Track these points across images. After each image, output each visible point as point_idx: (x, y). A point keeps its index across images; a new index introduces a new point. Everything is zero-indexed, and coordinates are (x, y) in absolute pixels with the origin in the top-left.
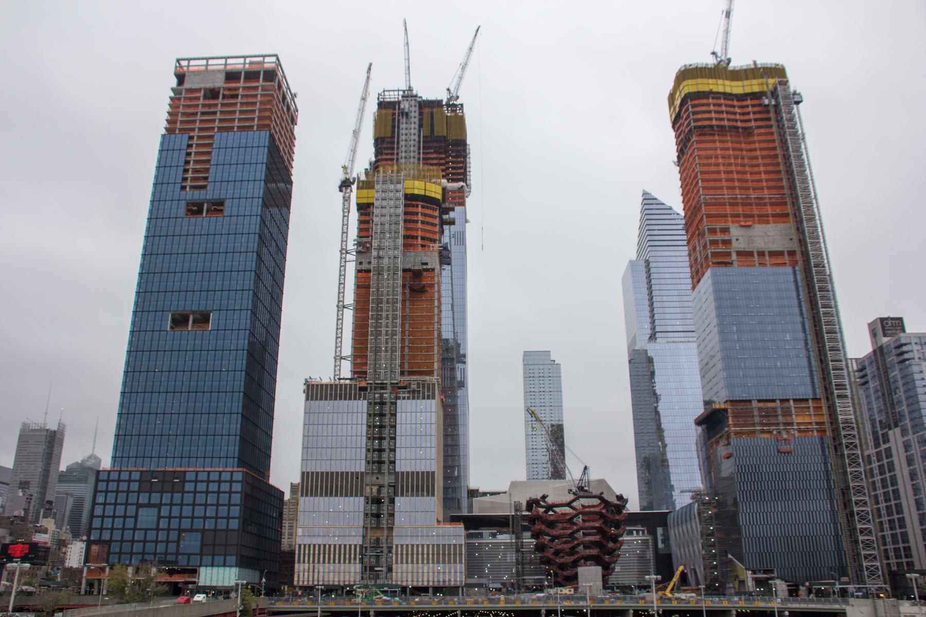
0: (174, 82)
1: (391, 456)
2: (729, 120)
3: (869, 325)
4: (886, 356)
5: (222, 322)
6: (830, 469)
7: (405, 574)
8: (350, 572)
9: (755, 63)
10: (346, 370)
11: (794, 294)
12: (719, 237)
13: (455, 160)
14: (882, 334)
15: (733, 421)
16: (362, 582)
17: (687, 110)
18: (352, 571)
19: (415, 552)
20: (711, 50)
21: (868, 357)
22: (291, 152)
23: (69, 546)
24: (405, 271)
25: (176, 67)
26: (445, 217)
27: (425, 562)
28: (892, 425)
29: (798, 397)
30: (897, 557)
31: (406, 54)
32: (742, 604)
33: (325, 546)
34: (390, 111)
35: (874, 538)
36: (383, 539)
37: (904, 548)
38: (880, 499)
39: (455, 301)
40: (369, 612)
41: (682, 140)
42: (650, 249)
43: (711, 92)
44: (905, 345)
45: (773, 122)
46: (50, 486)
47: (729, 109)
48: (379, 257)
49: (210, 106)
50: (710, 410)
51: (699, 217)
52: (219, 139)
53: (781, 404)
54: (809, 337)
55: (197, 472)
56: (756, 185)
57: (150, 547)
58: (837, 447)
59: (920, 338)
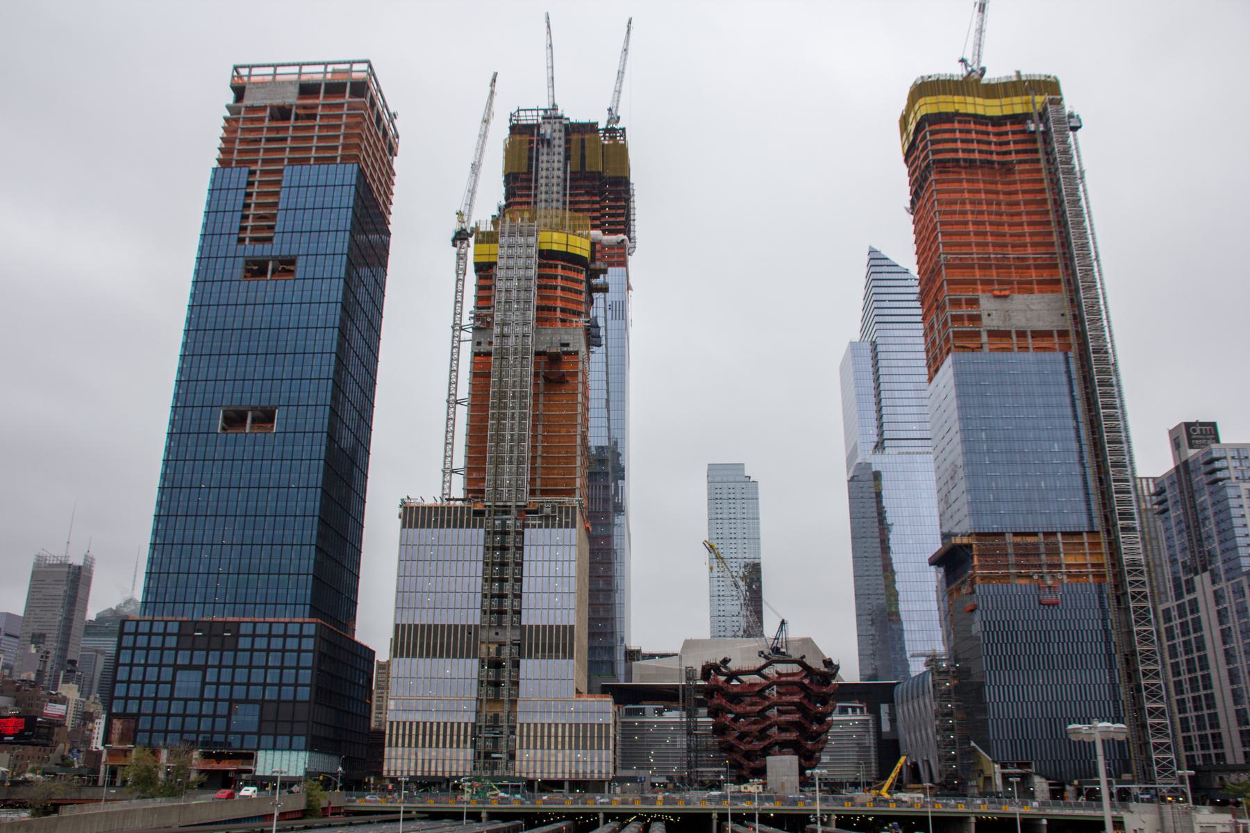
0: (230, 97)
1: (515, 603)
2: (980, 152)
3: (1171, 432)
4: (1193, 476)
5: (291, 422)
6: (1110, 628)
7: (532, 764)
8: (458, 760)
9: (1018, 73)
10: (458, 488)
11: (1066, 389)
12: (964, 311)
13: (613, 204)
15: (979, 561)
16: (474, 773)
17: (924, 137)
18: (462, 758)
19: (546, 734)
20: (960, 57)
21: (1168, 476)
22: (388, 193)
23: (97, 721)
24: (538, 354)
25: (233, 77)
26: (594, 281)
27: (560, 747)
29: (1068, 530)
30: (1203, 748)
31: (549, 60)
32: (984, 809)
33: (425, 724)
34: (526, 138)
35: (1168, 722)
36: (503, 716)
37: (1213, 735)
38: (1182, 668)
39: (612, 395)
40: (480, 813)
41: (916, 180)
42: (877, 326)
43: (957, 114)
44: (1218, 459)
45: (1041, 155)
46: (73, 640)
47: (980, 137)
48: (503, 336)
49: (278, 130)
50: (948, 546)
52: (290, 174)
53: (1045, 539)
54: (1085, 448)
55: (255, 623)
56: (1017, 241)
57: (191, 723)
58: (1120, 598)
59: (1238, 450)
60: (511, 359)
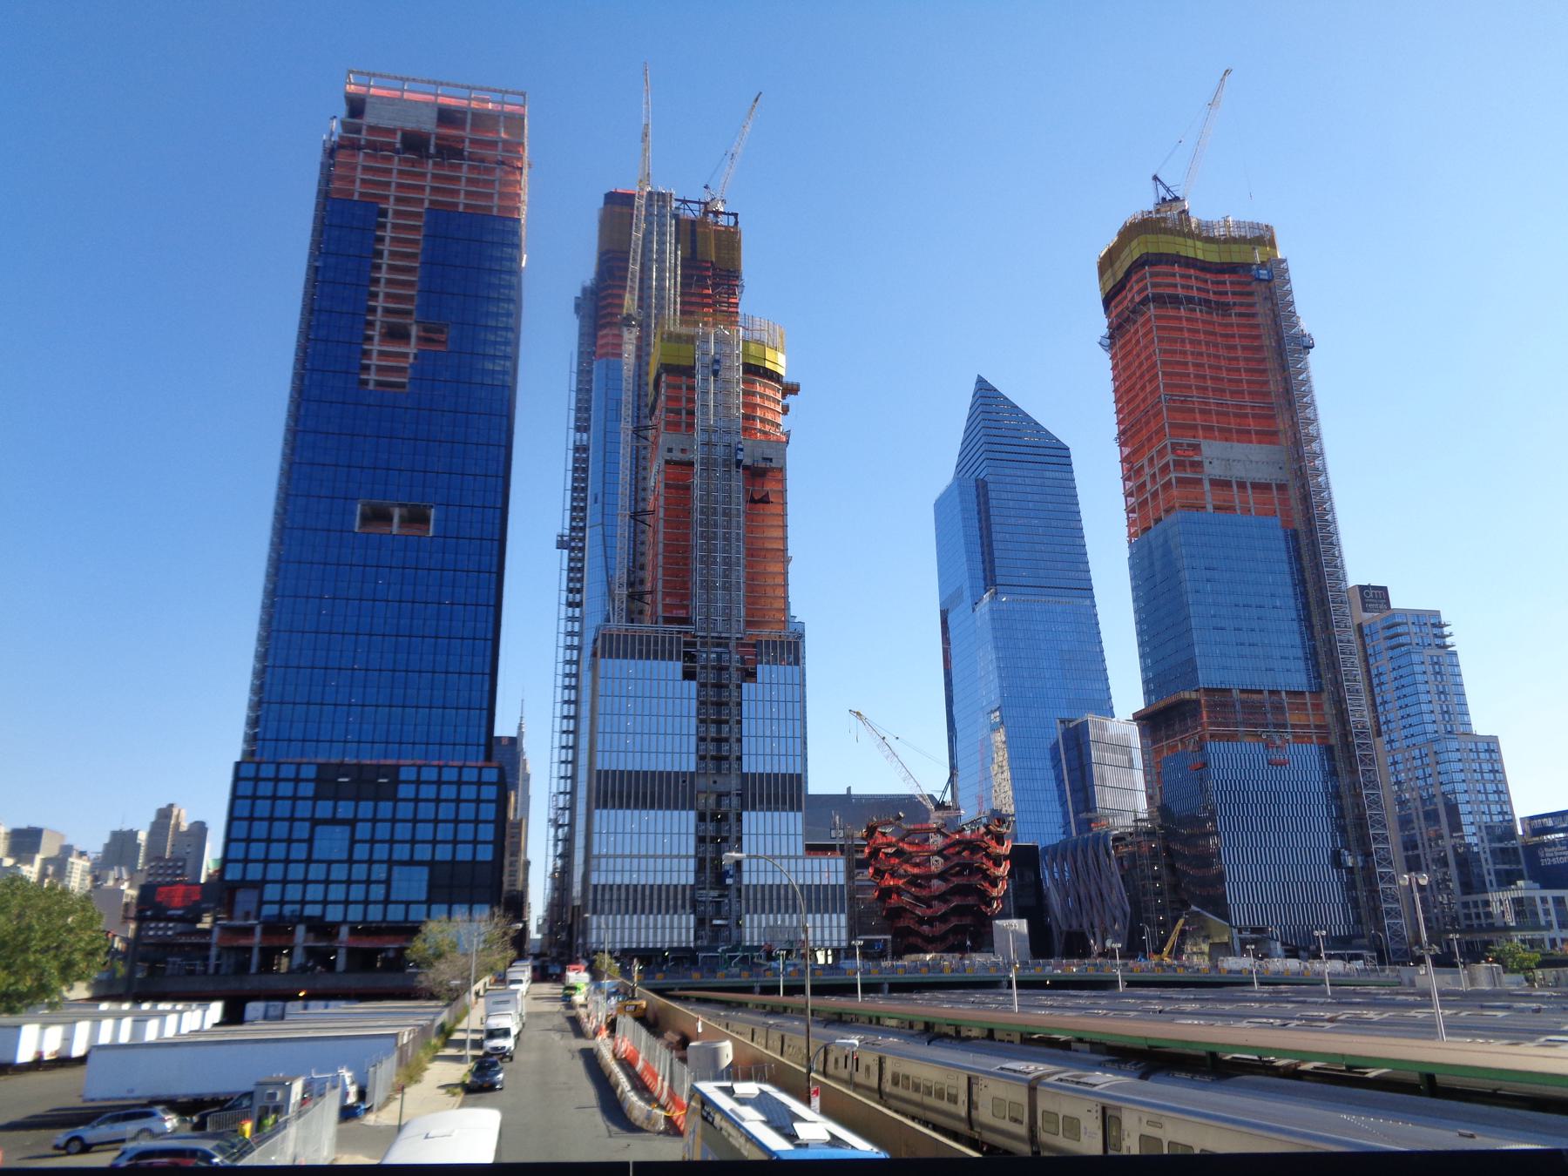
0: (342, 110)
15: (1209, 718)
29: (1245, 687)
44: (1399, 624)
59: (1418, 616)
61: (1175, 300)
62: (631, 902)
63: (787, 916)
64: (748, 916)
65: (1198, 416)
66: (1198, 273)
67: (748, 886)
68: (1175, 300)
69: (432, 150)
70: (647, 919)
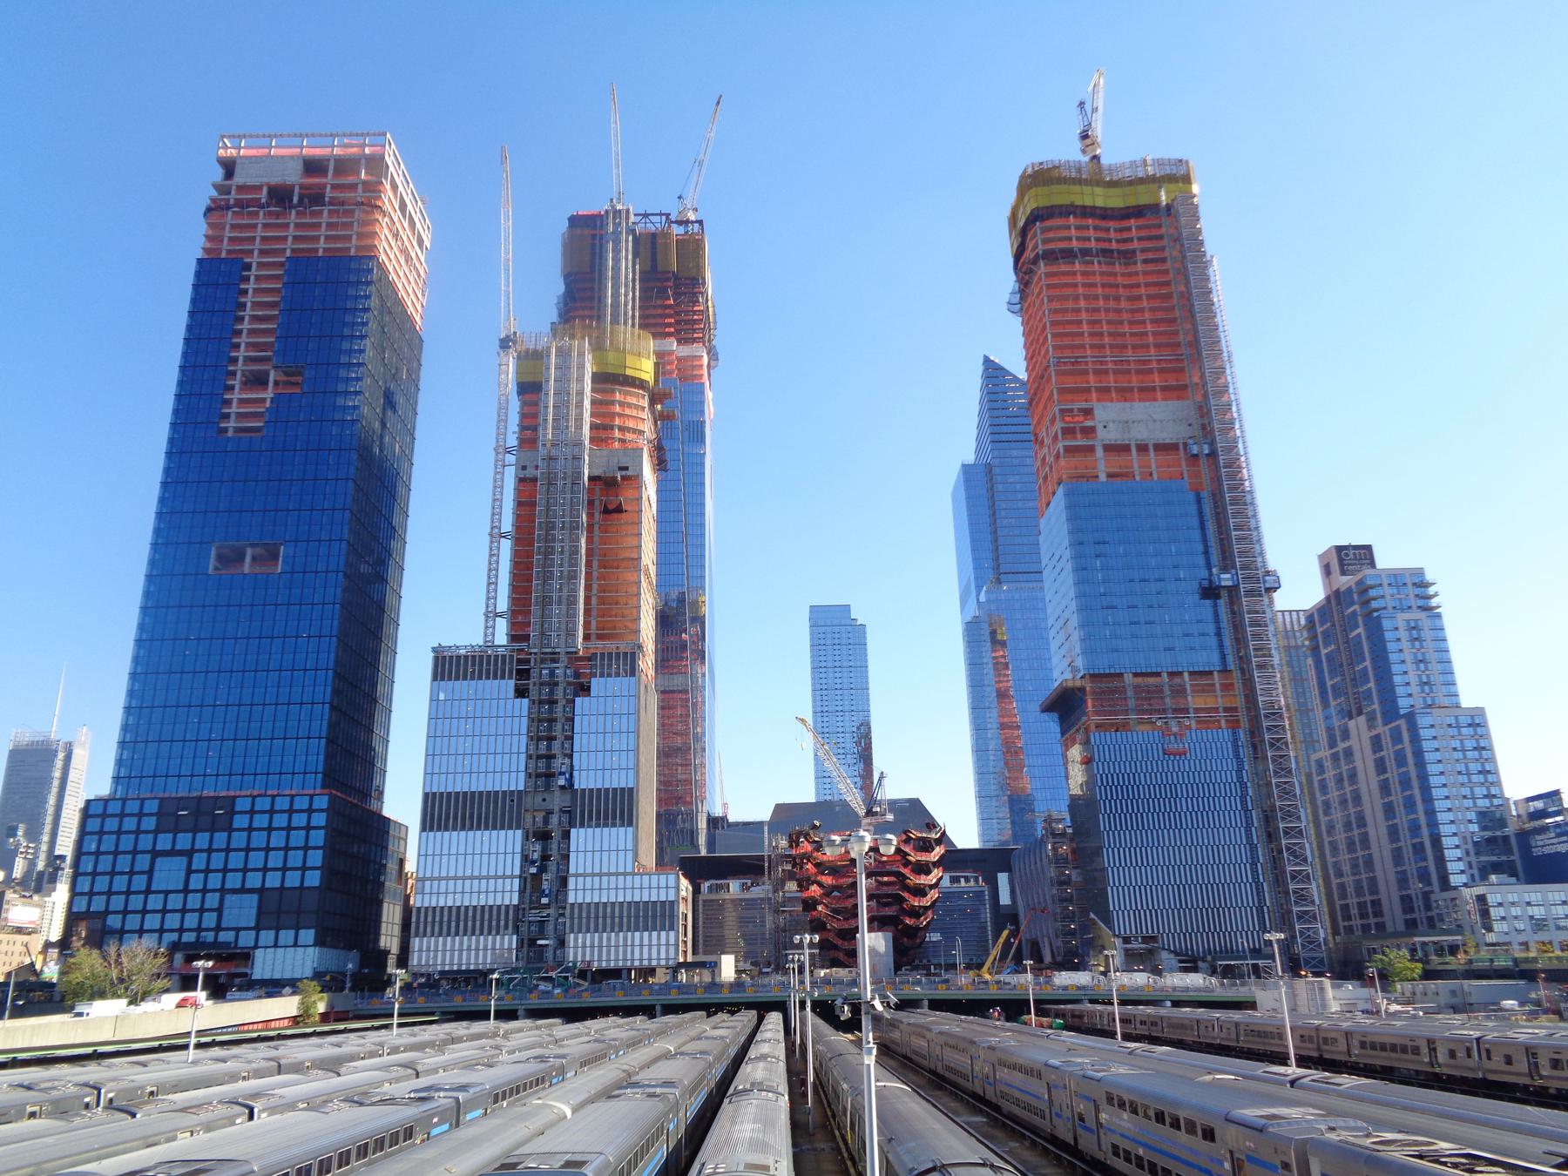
0: (218, 174)
10: (501, 638)
14: (1338, 572)
15: (1094, 706)
28: (1354, 712)
29: (1096, 672)
34: (587, 231)
51: (1047, 393)
60: (560, 483)
61: (1069, 255)
62: (453, 924)
63: (613, 934)
64: (572, 935)
65: (1091, 377)
66: (1099, 223)
67: (572, 904)
68: (1069, 255)
69: (295, 200)
70: (470, 940)
